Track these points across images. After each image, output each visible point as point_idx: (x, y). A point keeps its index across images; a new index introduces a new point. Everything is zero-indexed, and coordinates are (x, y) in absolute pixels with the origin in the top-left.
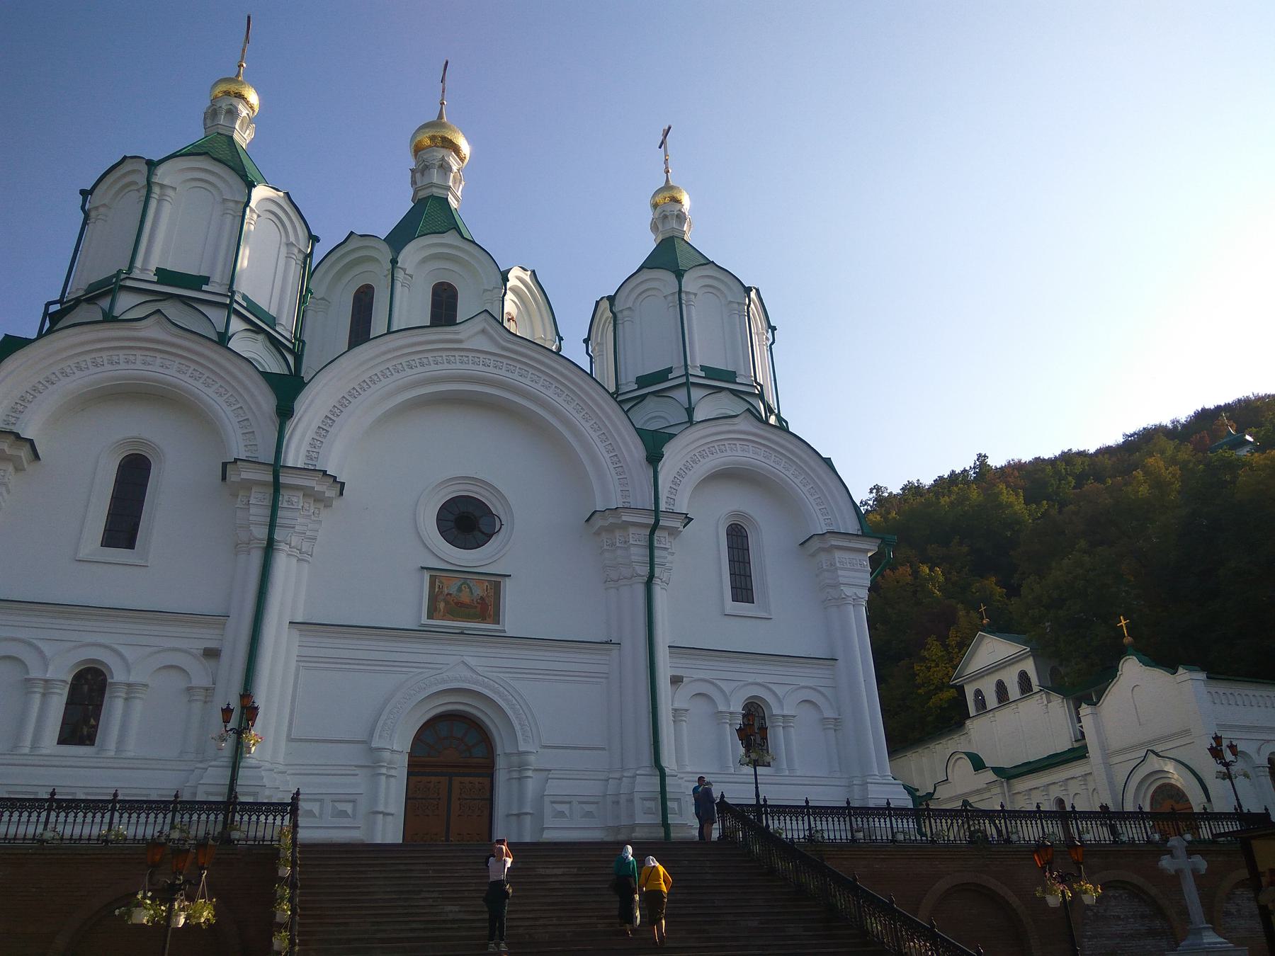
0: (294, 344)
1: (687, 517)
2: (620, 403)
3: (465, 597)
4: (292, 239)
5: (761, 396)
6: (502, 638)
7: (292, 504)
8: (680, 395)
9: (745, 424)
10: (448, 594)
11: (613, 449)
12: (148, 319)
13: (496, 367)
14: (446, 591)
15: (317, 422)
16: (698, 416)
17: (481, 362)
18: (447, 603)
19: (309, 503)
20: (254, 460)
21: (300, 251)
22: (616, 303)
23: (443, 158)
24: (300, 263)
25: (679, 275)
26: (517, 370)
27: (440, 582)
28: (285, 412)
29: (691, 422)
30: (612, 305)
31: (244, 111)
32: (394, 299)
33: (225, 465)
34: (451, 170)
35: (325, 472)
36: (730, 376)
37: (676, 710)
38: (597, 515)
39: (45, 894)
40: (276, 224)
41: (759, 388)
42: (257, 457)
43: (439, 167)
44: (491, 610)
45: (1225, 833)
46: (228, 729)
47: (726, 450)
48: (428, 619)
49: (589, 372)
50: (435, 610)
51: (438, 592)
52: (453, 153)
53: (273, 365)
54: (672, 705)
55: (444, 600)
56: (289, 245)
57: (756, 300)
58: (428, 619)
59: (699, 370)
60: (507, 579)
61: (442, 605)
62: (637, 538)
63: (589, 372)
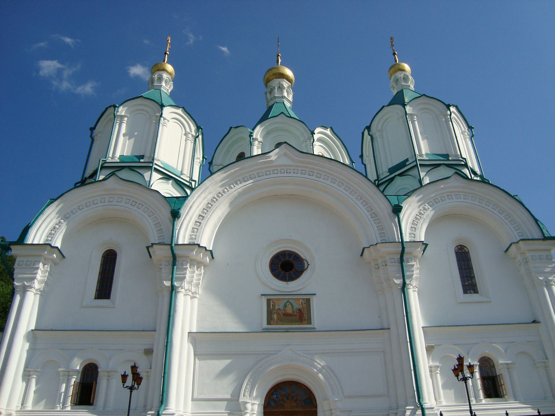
0: (191, 183)
1: (423, 244)
2: (378, 186)
3: (289, 310)
4: (188, 130)
5: (466, 165)
6: (313, 330)
8: (414, 172)
9: (456, 182)
10: (278, 309)
11: (372, 209)
12: (110, 178)
13: (324, 179)
14: (277, 307)
15: (195, 218)
17: (286, 172)
18: (278, 314)
20: (163, 243)
21: (192, 135)
23: (279, 83)
24: (193, 141)
25: (404, 105)
27: (273, 302)
28: (175, 215)
30: (369, 131)
31: (165, 76)
33: (148, 248)
34: (284, 88)
35: (199, 245)
36: (446, 156)
38: (366, 250)
40: (178, 124)
41: (464, 160)
42: (164, 242)
43: (278, 88)
44: (305, 316)
46: (125, 386)
47: (446, 200)
48: (267, 325)
49: (365, 175)
50: (271, 319)
51: (272, 308)
52: (285, 80)
53: (175, 193)
54: (428, 364)
55: (276, 313)
56: (185, 134)
57: (456, 112)
58: (267, 325)
60: (313, 296)
61: (275, 316)
62: (394, 268)
63: (365, 175)
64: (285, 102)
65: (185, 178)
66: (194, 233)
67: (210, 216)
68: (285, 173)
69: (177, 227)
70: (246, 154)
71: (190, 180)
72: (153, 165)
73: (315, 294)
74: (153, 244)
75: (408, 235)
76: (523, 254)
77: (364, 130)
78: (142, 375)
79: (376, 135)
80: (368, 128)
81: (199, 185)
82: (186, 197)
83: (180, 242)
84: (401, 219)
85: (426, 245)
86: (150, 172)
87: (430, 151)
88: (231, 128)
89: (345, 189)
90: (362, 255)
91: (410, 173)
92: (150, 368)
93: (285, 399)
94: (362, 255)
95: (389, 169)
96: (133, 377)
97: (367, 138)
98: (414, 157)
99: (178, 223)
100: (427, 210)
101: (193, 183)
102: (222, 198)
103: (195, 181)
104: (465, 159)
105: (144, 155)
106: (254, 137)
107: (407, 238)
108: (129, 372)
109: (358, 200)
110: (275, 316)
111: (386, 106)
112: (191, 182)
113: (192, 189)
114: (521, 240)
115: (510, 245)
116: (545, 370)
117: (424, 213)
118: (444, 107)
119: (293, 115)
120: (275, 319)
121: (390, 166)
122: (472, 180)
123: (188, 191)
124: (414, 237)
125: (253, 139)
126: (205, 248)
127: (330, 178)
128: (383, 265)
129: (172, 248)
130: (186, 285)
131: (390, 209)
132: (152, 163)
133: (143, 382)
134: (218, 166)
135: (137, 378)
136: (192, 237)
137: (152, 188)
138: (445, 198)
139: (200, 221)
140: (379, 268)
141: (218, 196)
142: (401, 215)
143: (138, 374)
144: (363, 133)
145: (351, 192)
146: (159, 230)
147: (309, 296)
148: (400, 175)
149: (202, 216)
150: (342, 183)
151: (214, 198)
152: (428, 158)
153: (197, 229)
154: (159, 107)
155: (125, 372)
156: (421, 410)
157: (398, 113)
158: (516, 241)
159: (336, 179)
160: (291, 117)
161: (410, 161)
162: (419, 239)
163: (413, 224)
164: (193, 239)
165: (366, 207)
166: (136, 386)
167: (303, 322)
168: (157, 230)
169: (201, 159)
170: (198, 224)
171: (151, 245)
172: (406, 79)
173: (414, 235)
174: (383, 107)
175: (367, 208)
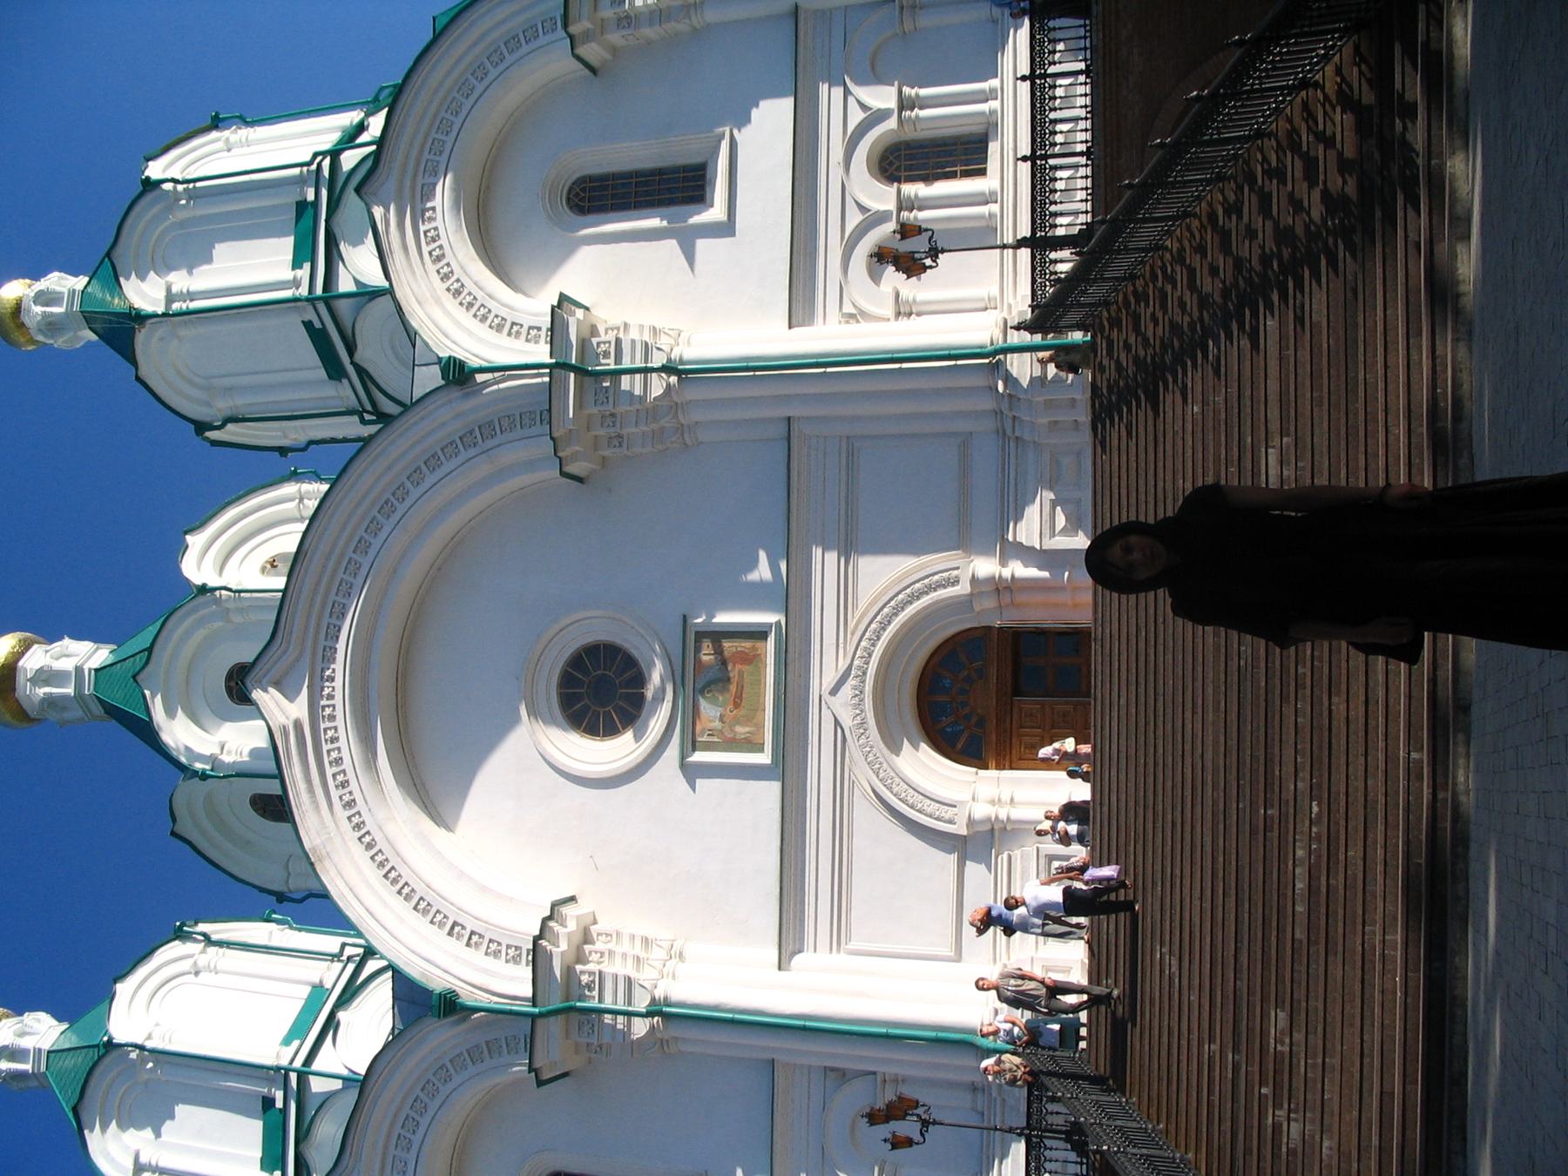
0: (349, 959)
4: (186, 965)
5: (335, 154)
7: (593, 982)
10: (722, 719)
14: (717, 724)
16: (376, 278)
18: (736, 721)
19: (598, 344)
20: (528, 1040)
22: (207, 419)
26: (339, 599)
28: (449, 1005)
29: (390, 292)
32: (258, 772)
33: (540, 1083)
35: (536, 940)
37: (898, 314)
38: (567, 469)
39: (1190, 1155)
45: (1138, 523)
47: (436, 229)
59: (285, 1049)
61: (741, 730)
64: (96, 666)
65: (332, 975)
66: (500, 951)
67: (452, 904)
68: (333, 684)
69: (485, 1000)
70: (259, 792)
71: (339, 961)
72: (294, 1070)
73: (685, 616)
74: (531, 1069)
75: (531, 346)
76: (603, 26)
77: (207, 439)
78: (890, 1096)
79: (223, 406)
80: (201, 427)
81: (360, 935)
82: (391, 967)
83: (528, 992)
84: (485, 364)
85: (562, 295)
86: (311, 1077)
87: (281, 234)
88: (173, 833)
89: (389, 516)
90: (579, 480)
91: (347, 322)
92: (873, 1076)
93: (967, 710)
94: (579, 480)
95: (330, 377)
96: (896, 1119)
97: (232, 433)
98: (299, 304)
99: (468, 996)
100: (463, 286)
101: (349, 951)
102: (402, 869)
103: (344, 945)
104: (316, 155)
105: (263, 1097)
106: (208, 767)
107: (541, 353)
108: (885, 1130)
109: (423, 479)
110: (741, 730)
111: (137, 369)
112: (344, 958)
113: (370, 952)
114: (565, 25)
115: (578, 58)
116: (921, 8)
117: (470, 294)
118: (149, 197)
119: (143, 640)
120: (747, 729)
121: (322, 373)
122: (381, 142)
123: (372, 966)
124: (539, 329)
125: (212, 770)
126: (545, 921)
127: (354, 556)
128: (613, 422)
129: (541, 1015)
130: (645, 976)
131: (455, 393)
132: (287, 1071)
133: (909, 1092)
134: (289, 874)
135: (899, 1109)
136: (513, 957)
137: (363, 1072)
138: (429, 231)
139: (467, 934)
140: (620, 436)
141: (395, 882)
142: (474, 362)
143: (890, 1106)
144: (215, 443)
145: (398, 499)
146: (490, 1053)
147: (688, 633)
148: (351, 350)
149: (452, 928)
150: (371, 522)
151: (399, 892)
152: (305, 265)
153: (491, 941)
154: (115, 1054)
155: (885, 1141)
156: (1009, 356)
157: (161, 339)
158: (569, 40)
159: (357, 539)
160: (150, 650)
161: (310, 315)
162: (545, 315)
163: (499, 328)
164: (520, 955)
165: (442, 458)
166: (920, 1111)
167: (759, 655)
168: (491, 1058)
169: (272, 926)
170: (457, 929)
171: (533, 1074)
172: (45, 298)
173: (530, 328)
174: (138, 379)
175: (448, 456)
